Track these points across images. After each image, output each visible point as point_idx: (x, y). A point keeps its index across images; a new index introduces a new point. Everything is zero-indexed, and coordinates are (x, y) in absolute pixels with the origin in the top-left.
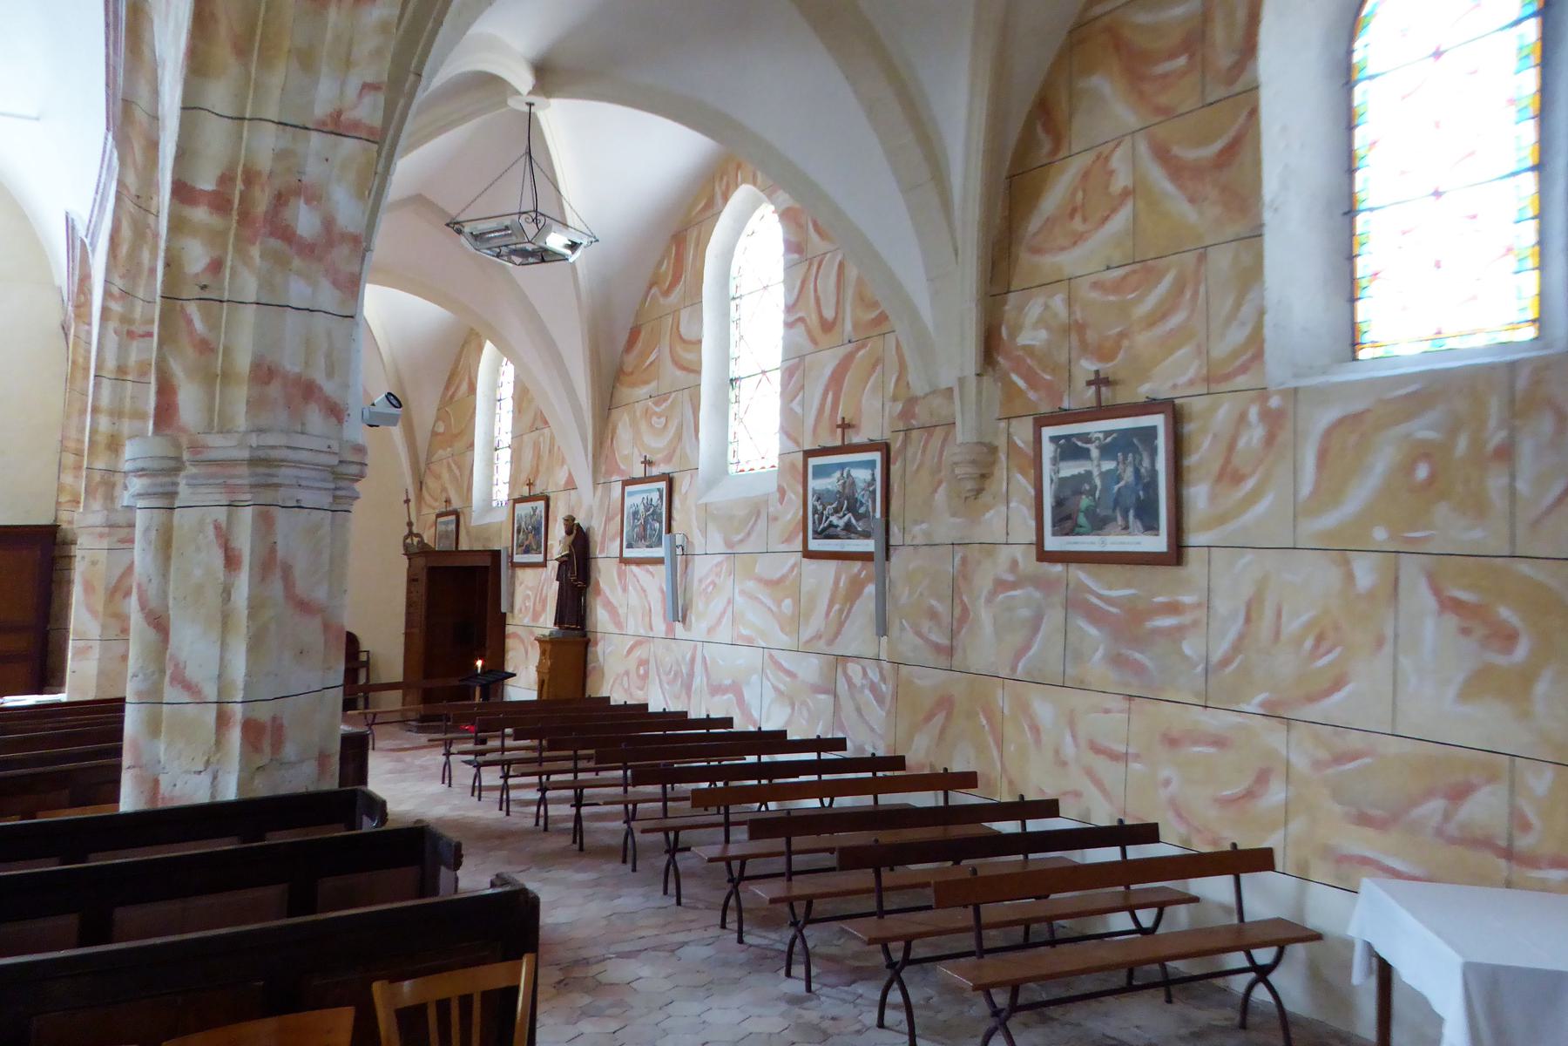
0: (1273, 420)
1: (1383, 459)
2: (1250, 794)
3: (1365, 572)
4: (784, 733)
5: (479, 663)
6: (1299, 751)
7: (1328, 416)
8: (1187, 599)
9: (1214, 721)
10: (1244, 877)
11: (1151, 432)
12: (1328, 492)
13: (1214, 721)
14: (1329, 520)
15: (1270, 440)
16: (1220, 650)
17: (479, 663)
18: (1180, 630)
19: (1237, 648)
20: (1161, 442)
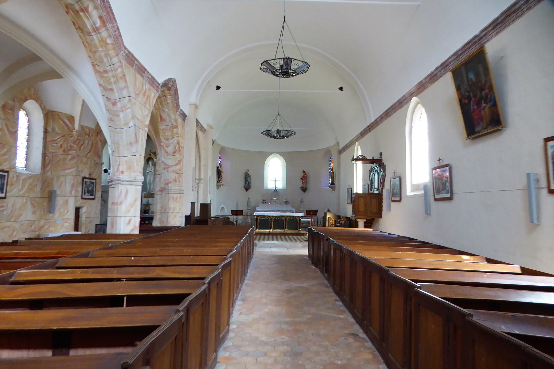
0: (17, 176)
1: (27, 184)
2: (12, 234)
3: (25, 201)
4: (186, 217)
5: (483, 360)
6: (17, 225)
7: (22, 178)
8: (5, 205)
9: (7, 224)
10: (307, 243)
11: (4, 176)
12: (22, 189)
13: (7, 224)
14: (21, 193)
15: (17, 180)
16: (9, 212)
17: (483, 360)
18: (4, 210)
19: (11, 212)
20: (6, 178)
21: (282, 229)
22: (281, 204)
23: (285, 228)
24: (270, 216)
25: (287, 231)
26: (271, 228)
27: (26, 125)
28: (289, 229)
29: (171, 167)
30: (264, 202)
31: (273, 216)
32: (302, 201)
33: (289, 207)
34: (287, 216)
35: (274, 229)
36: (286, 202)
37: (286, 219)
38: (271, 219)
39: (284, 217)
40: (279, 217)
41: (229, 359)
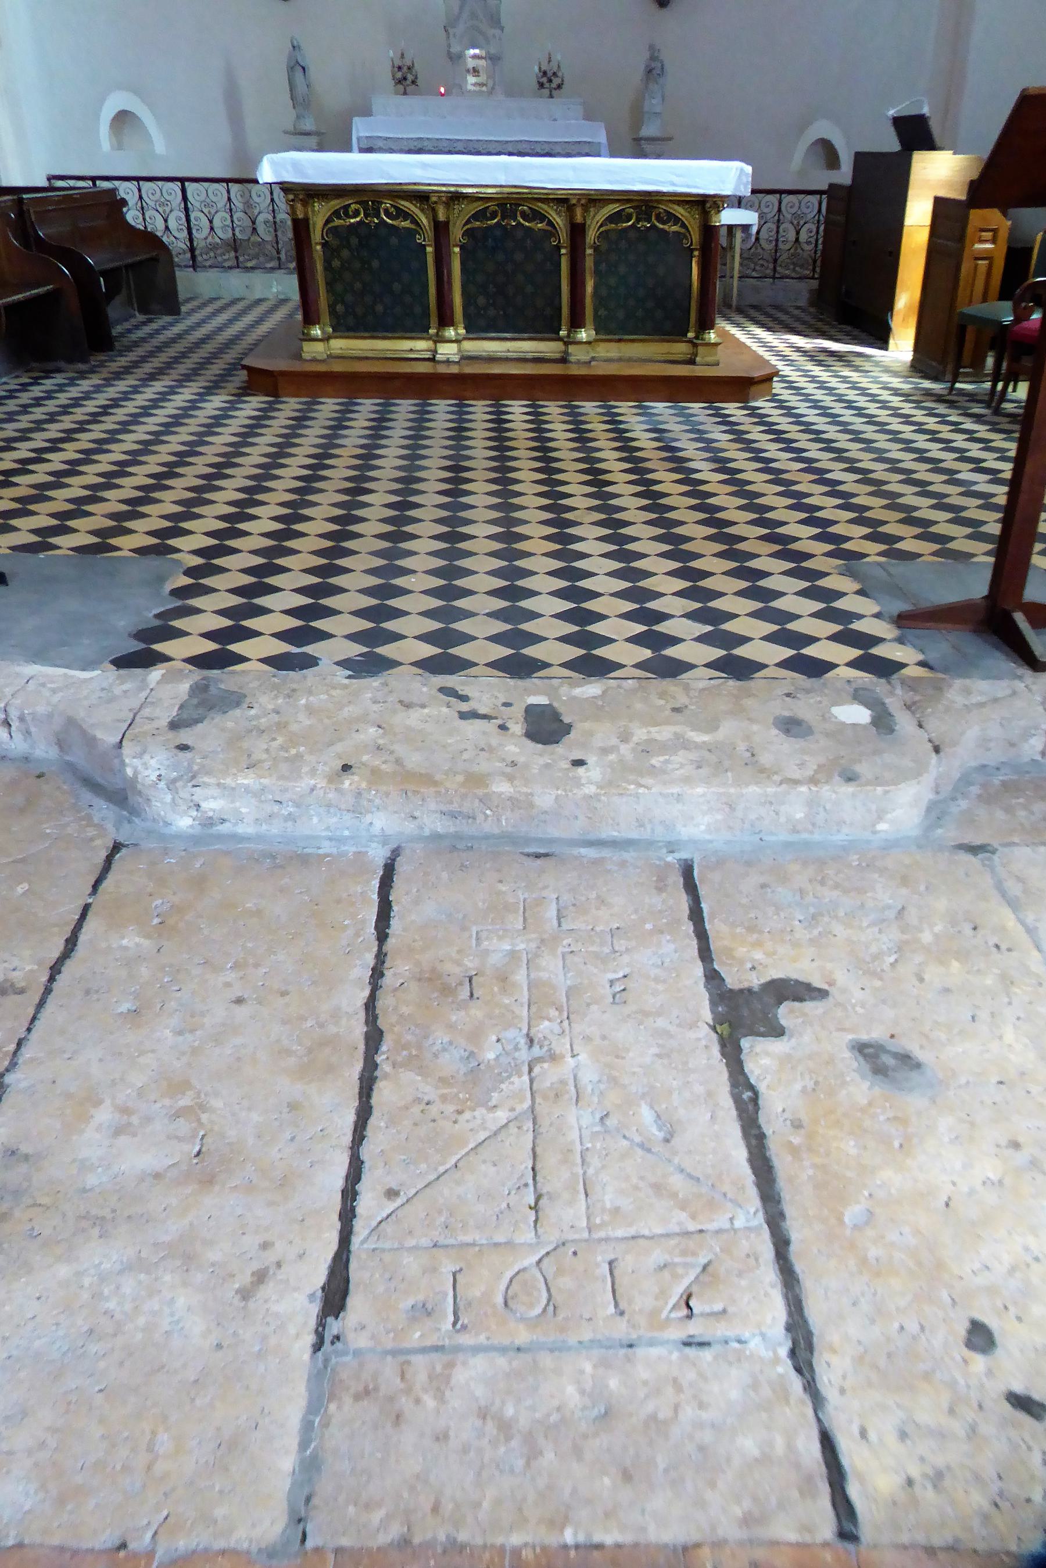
21: (544, 325)
22: (512, 91)
23: (576, 323)
24: (421, 197)
25: (590, 349)
26: (445, 320)
27: (418, 348)
28: (611, 328)
29: (234, 235)
30: (405, 79)
31: (455, 198)
32: (653, 71)
33: (561, 118)
34: (594, 199)
35: (476, 327)
36: (549, 82)
37: (577, 231)
38: (441, 229)
39: (564, 201)
40: (513, 204)
41: (32, 1060)
